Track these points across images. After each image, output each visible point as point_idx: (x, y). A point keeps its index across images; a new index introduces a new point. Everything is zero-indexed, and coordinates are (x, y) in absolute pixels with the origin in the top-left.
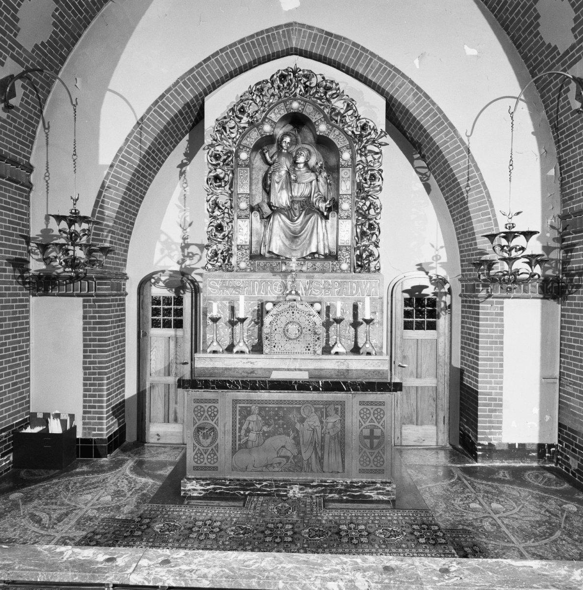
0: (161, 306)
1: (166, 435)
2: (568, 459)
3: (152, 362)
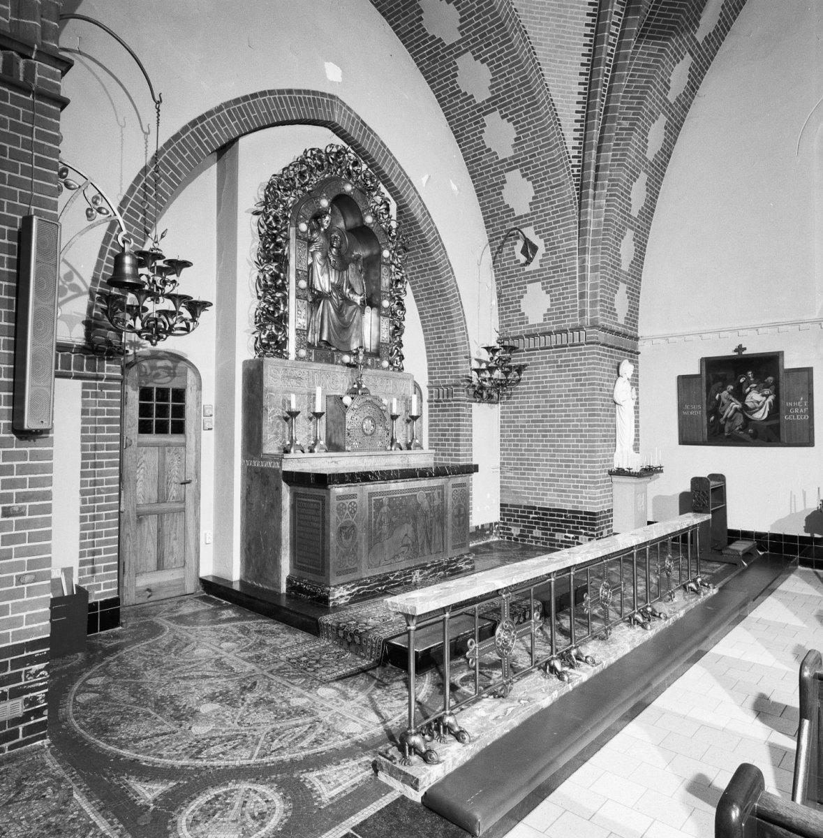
0: (171, 403)
1: (160, 587)
2: (509, 529)
3: (139, 484)
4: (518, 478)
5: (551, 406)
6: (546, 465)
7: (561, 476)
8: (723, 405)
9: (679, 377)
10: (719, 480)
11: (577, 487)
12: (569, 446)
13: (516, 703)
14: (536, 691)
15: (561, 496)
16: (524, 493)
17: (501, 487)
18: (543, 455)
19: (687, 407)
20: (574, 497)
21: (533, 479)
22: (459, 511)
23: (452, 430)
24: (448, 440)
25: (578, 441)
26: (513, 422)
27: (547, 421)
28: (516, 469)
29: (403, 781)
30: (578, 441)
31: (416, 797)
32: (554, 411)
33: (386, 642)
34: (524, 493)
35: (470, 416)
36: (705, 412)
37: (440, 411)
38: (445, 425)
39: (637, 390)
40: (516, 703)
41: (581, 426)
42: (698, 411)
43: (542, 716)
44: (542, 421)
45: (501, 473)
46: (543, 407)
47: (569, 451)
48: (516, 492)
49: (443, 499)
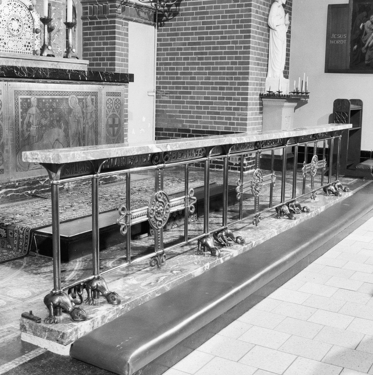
4: (174, 102)
5: (208, 28)
6: (201, 88)
7: (215, 98)
8: (366, 34)
9: (329, 5)
10: (357, 105)
11: (230, 109)
12: (224, 69)
13: (169, 273)
14: (190, 264)
15: (215, 118)
16: (179, 117)
17: (157, 111)
18: (199, 78)
19: (334, 36)
20: (227, 119)
21: (188, 103)
22: (114, 121)
23: (107, 49)
24: (103, 59)
25: (233, 63)
26: (170, 45)
27: (204, 44)
28: (172, 93)
29: (48, 338)
30: (233, 63)
31: (64, 351)
32: (211, 33)
33: (33, 231)
34: (179, 117)
35: (127, 35)
36: (349, 41)
37: (95, 28)
38: (100, 44)
39: (290, 14)
40: (169, 273)
41: (237, 48)
42: (344, 40)
43: (195, 282)
44: (199, 44)
45: (157, 97)
46: (200, 28)
47: (224, 73)
48: (171, 116)
49: (96, 107)
